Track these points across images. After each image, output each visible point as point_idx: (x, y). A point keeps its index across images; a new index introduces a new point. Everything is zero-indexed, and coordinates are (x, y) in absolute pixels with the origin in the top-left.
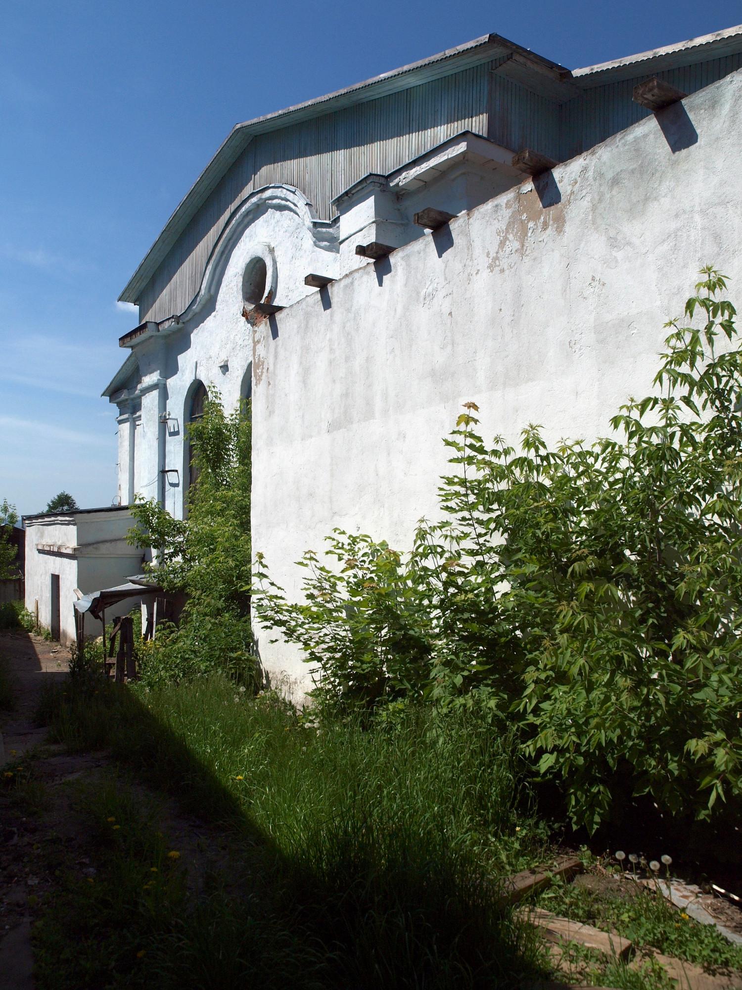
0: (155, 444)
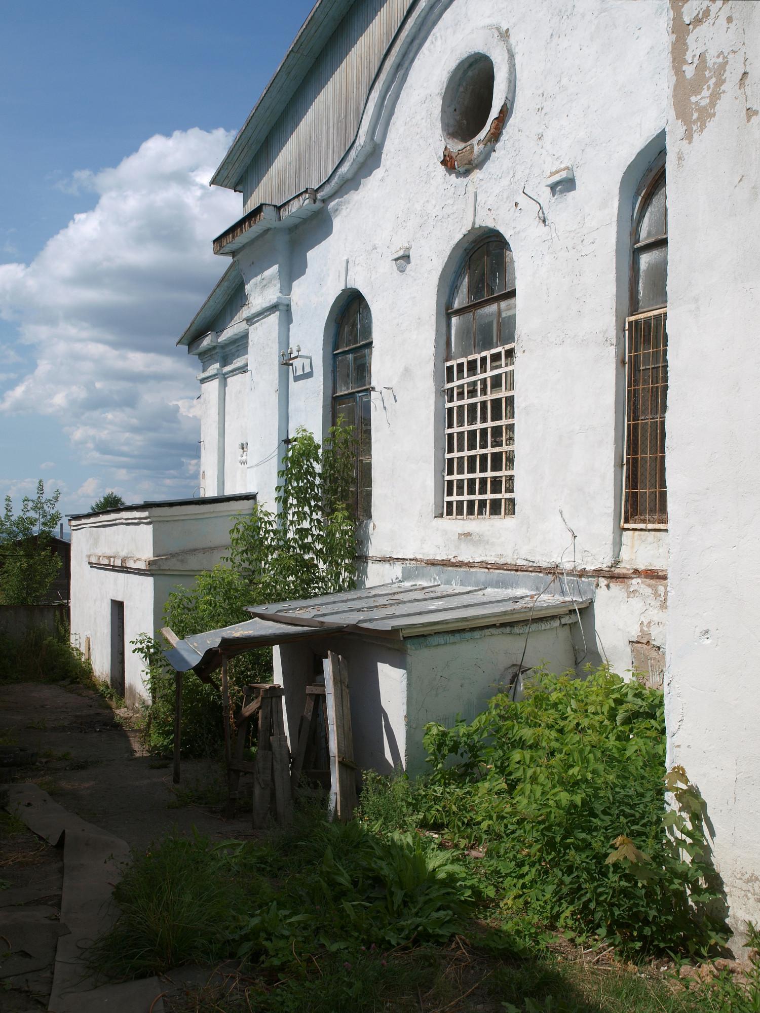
0: (274, 399)
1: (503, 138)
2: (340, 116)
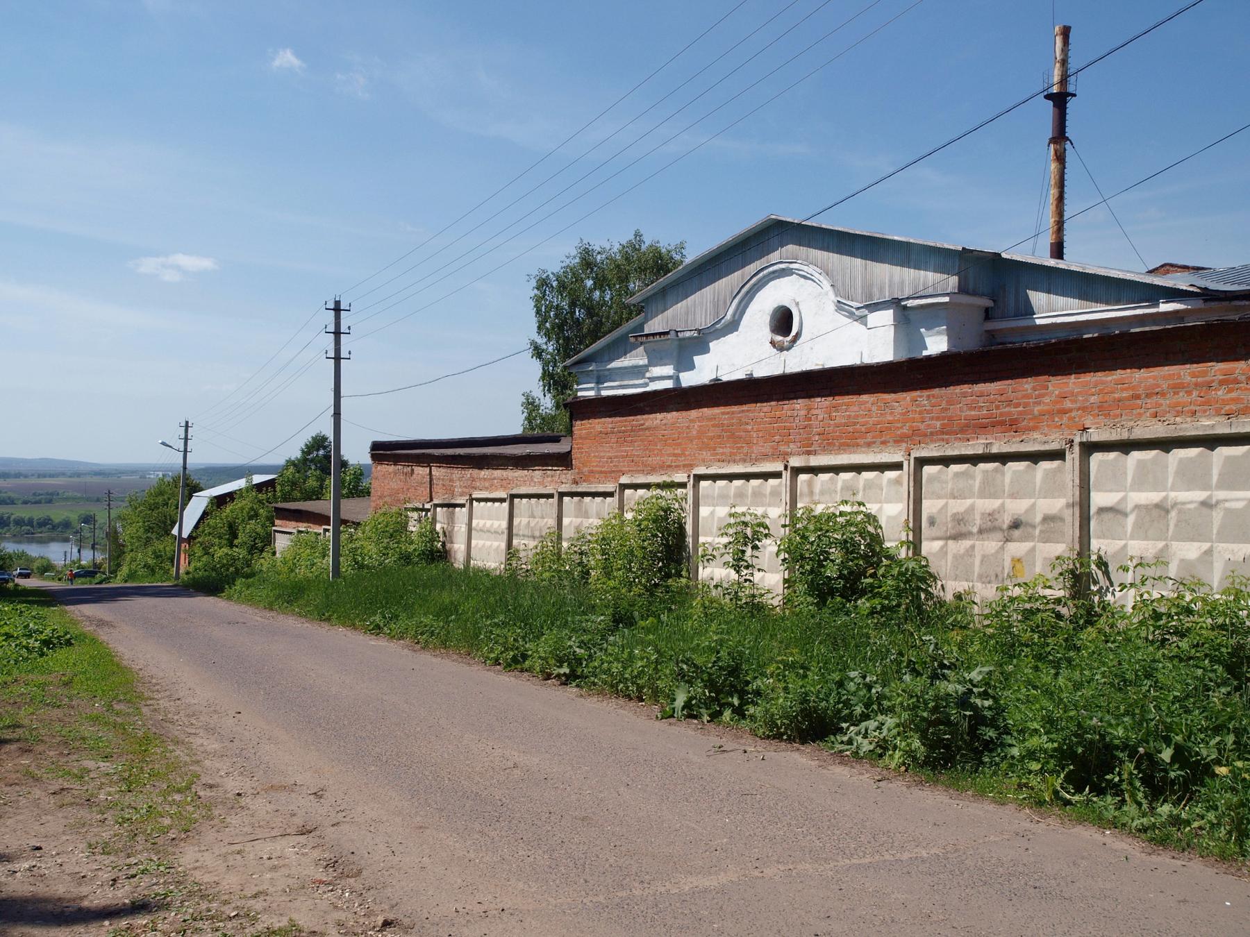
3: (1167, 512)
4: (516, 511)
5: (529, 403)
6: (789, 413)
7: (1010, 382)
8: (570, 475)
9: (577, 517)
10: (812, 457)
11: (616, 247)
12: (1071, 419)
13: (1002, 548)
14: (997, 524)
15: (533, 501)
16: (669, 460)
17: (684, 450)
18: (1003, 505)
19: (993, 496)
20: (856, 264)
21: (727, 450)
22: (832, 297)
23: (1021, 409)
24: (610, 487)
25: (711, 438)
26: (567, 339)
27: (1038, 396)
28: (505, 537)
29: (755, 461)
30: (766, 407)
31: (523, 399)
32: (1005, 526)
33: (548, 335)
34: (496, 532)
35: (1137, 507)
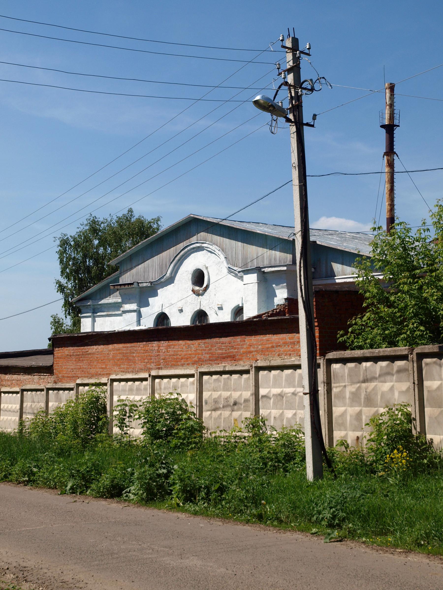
1: (208, 291)
2: (160, 263)
3: (283, 397)
4: (25, 399)
5: (56, 322)
6: (151, 348)
7: (232, 338)
8: (51, 379)
9: (56, 402)
10: (160, 371)
11: (115, 218)
12: (253, 355)
13: (231, 414)
14: (228, 403)
15: (34, 393)
16: (99, 371)
17: (106, 365)
18: (221, 393)
19: (228, 390)
20: (238, 246)
21: (126, 366)
22: (225, 265)
23: (236, 350)
24: (72, 385)
25: (118, 360)
26: (80, 280)
27: (242, 345)
28: (18, 414)
29: (137, 372)
30: (142, 344)
31: (52, 319)
32: (232, 404)
33: (68, 277)
34: (14, 411)
35: (273, 395)
